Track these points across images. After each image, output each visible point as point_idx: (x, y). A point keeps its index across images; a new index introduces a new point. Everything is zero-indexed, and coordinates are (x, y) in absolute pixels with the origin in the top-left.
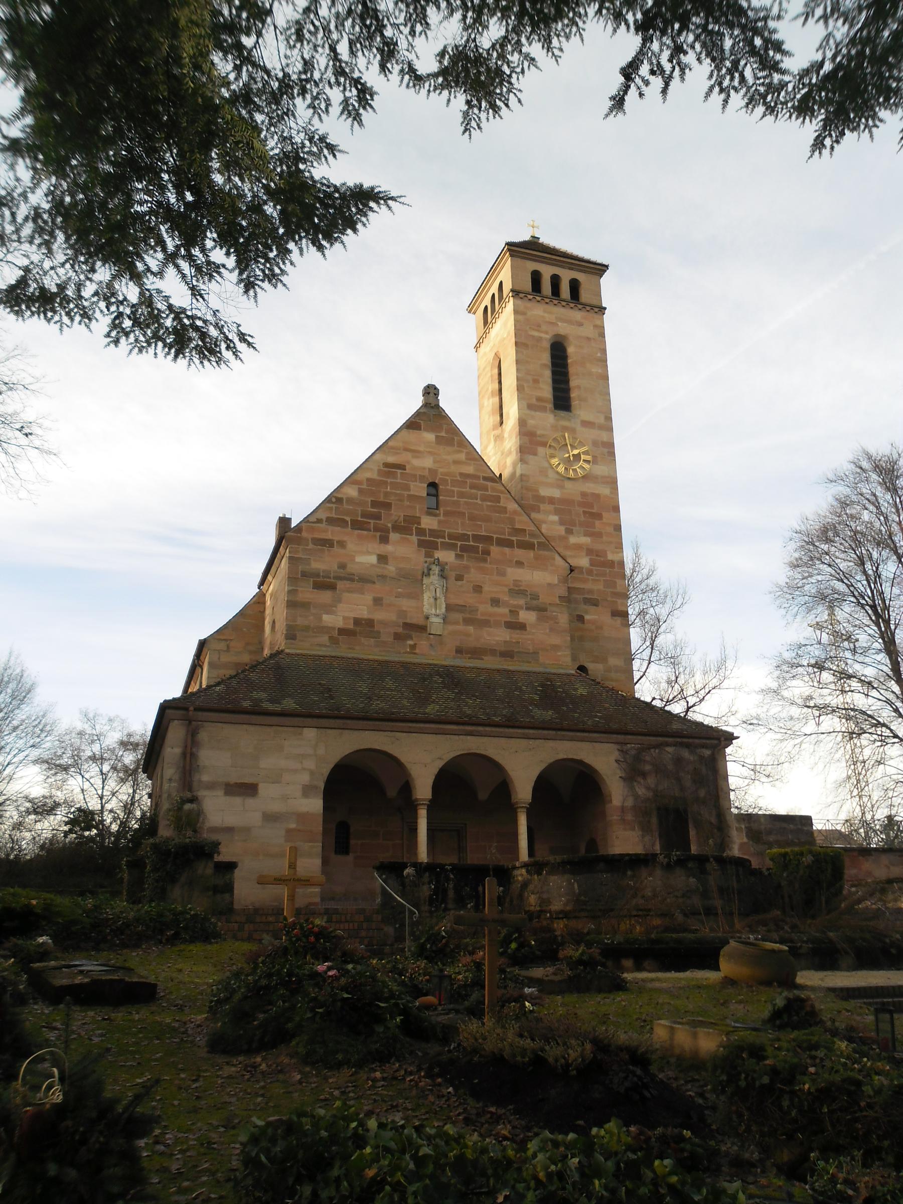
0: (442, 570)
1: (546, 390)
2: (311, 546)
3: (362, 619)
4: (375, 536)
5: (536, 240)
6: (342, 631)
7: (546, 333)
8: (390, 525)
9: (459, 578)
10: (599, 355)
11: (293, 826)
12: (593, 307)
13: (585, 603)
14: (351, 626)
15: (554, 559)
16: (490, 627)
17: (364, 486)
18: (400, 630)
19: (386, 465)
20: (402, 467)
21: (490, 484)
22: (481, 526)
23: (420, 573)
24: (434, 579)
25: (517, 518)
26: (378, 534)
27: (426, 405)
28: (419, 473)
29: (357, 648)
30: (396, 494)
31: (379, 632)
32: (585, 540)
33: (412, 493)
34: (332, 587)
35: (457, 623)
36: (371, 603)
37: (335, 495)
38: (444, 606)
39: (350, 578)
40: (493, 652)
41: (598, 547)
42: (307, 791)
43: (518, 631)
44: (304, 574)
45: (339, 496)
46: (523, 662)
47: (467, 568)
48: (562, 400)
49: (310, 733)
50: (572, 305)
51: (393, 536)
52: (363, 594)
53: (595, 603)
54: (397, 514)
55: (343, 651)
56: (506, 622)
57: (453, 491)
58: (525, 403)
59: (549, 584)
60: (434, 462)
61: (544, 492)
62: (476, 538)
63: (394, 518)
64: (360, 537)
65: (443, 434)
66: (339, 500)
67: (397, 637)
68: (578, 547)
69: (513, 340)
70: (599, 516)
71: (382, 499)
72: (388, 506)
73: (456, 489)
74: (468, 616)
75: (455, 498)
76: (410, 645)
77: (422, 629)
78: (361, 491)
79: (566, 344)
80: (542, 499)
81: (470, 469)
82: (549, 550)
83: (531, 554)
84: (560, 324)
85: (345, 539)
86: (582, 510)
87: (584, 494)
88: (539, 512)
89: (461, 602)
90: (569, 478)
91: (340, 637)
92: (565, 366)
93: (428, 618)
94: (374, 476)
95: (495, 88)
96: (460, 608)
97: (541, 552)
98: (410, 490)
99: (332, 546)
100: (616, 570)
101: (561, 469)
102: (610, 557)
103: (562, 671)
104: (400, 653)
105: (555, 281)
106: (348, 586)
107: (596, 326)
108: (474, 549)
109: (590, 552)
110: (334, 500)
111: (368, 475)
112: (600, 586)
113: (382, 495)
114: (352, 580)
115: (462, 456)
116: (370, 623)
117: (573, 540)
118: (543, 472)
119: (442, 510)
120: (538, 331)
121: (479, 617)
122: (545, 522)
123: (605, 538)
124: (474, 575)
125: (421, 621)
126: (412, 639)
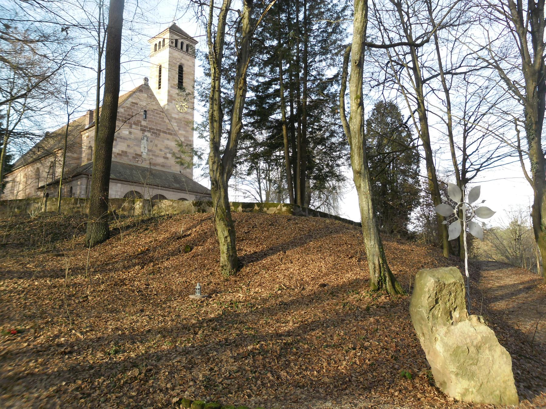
6: (118, 154)
9: (151, 142)
19: (132, 103)
20: (137, 104)
24: (144, 141)
32: (184, 132)
39: (121, 138)
40: (159, 165)
49: (119, 185)
51: (134, 126)
62: (157, 130)
63: (134, 120)
67: (133, 157)
68: (181, 134)
69: (168, 63)
77: (141, 156)
78: (125, 111)
92: (182, 74)
95: (247, 109)
101: (179, 109)
108: (156, 133)
109: (185, 136)
116: (126, 152)
117: (180, 132)
118: (173, 109)
125: (140, 154)
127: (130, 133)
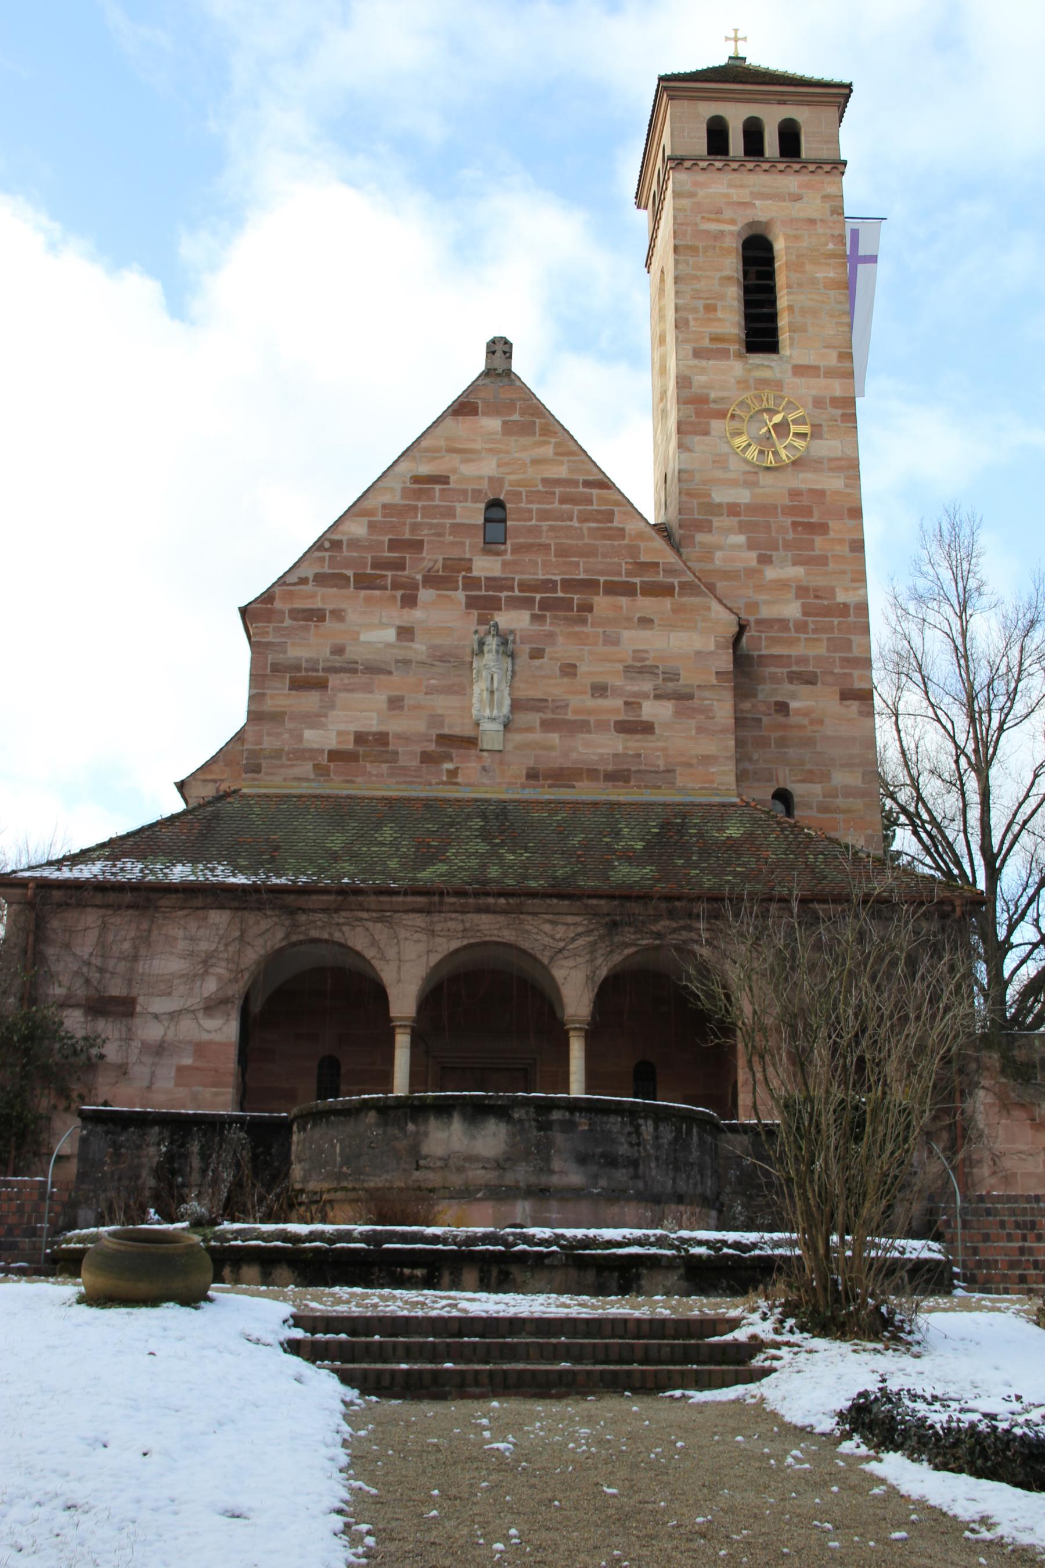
0: (505, 643)
1: (730, 320)
2: (288, 622)
3: (368, 734)
4: (394, 597)
5: (738, 63)
6: (335, 755)
7: (733, 222)
8: (419, 577)
9: (537, 654)
10: (831, 246)
11: (188, 1061)
12: (819, 164)
13: (791, 682)
14: (350, 746)
15: (709, 609)
16: (589, 732)
17: (379, 518)
18: (432, 747)
19: (416, 479)
20: (442, 480)
21: (595, 492)
22: (577, 564)
23: (468, 650)
25: (642, 545)
26: (399, 594)
27: (488, 373)
28: (471, 487)
29: (359, 779)
30: (431, 526)
31: (396, 753)
32: (797, 572)
33: (458, 520)
34: (321, 685)
35: (530, 729)
36: (385, 706)
37: (329, 536)
38: (507, 702)
39: (350, 669)
40: (592, 774)
41: (820, 581)
42: (212, 1006)
43: (639, 737)
44: (276, 668)
45: (336, 537)
46: (646, 787)
47: (551, 636)
48: (761, 334)
50: (750, 165)
51: (425, 595)
52: (371, 692)
53: (810, 680)
54: (432, 558)
55: (337, 787)
56: (616, 723)
57: (530, 511)
58: (689, 348)
59: (698, 653)
60: (499, 466)
61: (721, 496)
62: (569, 585)
63: (427, 564)
64: (368, 600)
65: (516, 417)
66: (336, 545)
67: (427, 758)
68: (782, 585)
70: (822, 528)
71: (407, 536)
72: (417, 545)
73: (534, 507)
74: (550, 716)
75: (533, 522)
76: (448, 771)
78: (372, 526)
79: (770, 238)
80: (715, 509)
81: (561, 471)
82: (700, 594)
83: (667, 603)
84: (757, 203)
85: (344, 606)
86: (789, 520)
87: (794, 493)
88: (710, 531)
89: (539, 695)
90: (768, 469)
91: (332, 765)
93: (478, 725)
94: (397, 499)
96: (536, 705)
97: (685, 599)
98: (454, 516)
99: (322, 618)
100: (851, 619)
101: (752, 454)
102: (841, 597)
103: (716, 800)
104: (430, 784)
105: (753, 133)
106: (346, 681)
107: (826, 197)
108: (565, 605)
109: (802, 591)
110: (327, 545)
111: (387, 499)
112: (821, 650)
113: (407, 529)
114: (354, 671)
115: (548, 451)
116: (382, 738)
117: (771, 573)
118: (720, 462)
119: (509, 542)
120: (718, 221)
121: (570, 716)
122: (720, 548)
123: (832, 566)
124: (563, 648)
126: (451, 760)
127: (405, 633)
